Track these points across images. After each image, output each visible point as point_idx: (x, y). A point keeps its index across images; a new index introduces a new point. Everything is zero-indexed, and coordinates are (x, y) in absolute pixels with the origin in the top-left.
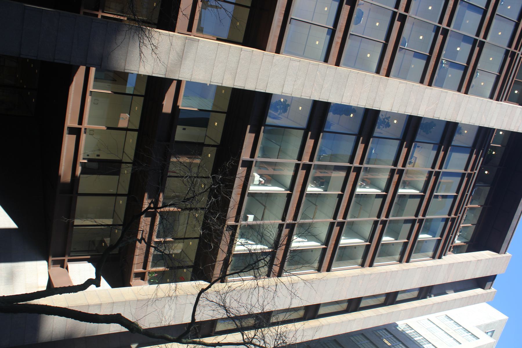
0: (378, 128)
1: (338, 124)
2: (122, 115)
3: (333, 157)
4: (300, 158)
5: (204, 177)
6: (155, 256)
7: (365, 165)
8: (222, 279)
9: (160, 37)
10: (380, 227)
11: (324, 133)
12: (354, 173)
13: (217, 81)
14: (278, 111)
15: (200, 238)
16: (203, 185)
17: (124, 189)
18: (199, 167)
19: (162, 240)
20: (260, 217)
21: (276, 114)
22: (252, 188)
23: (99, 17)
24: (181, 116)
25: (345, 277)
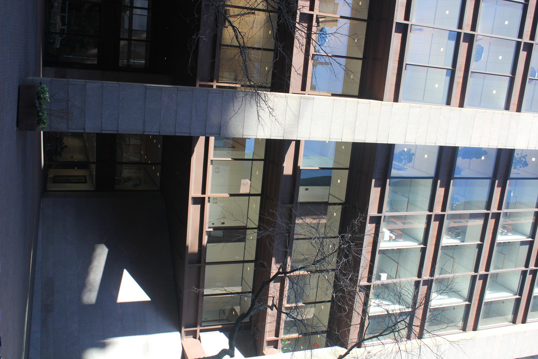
0: (514, 169)
1: (469, 169)
2: (243, 181)
3: (467, 205)
4: (431, 209)
5: (332, 237)
6: (286, 322)
7: (504, 210)
8: (358, 345)
9: (275, 98)
10: (529, 277)
11: (511, 180)
12: (492, 220)
13: (336, 137)
14: (402, 162)
15: (332, 301)
16: (331, 246)
17: (251, 255)
18: (325, 227)
19: (294, 305)
20: (393, 274)
21: (401, 165)
22: (383, 245)
23: (215, 87)
24: (303, 176)
25: (495, 336)
